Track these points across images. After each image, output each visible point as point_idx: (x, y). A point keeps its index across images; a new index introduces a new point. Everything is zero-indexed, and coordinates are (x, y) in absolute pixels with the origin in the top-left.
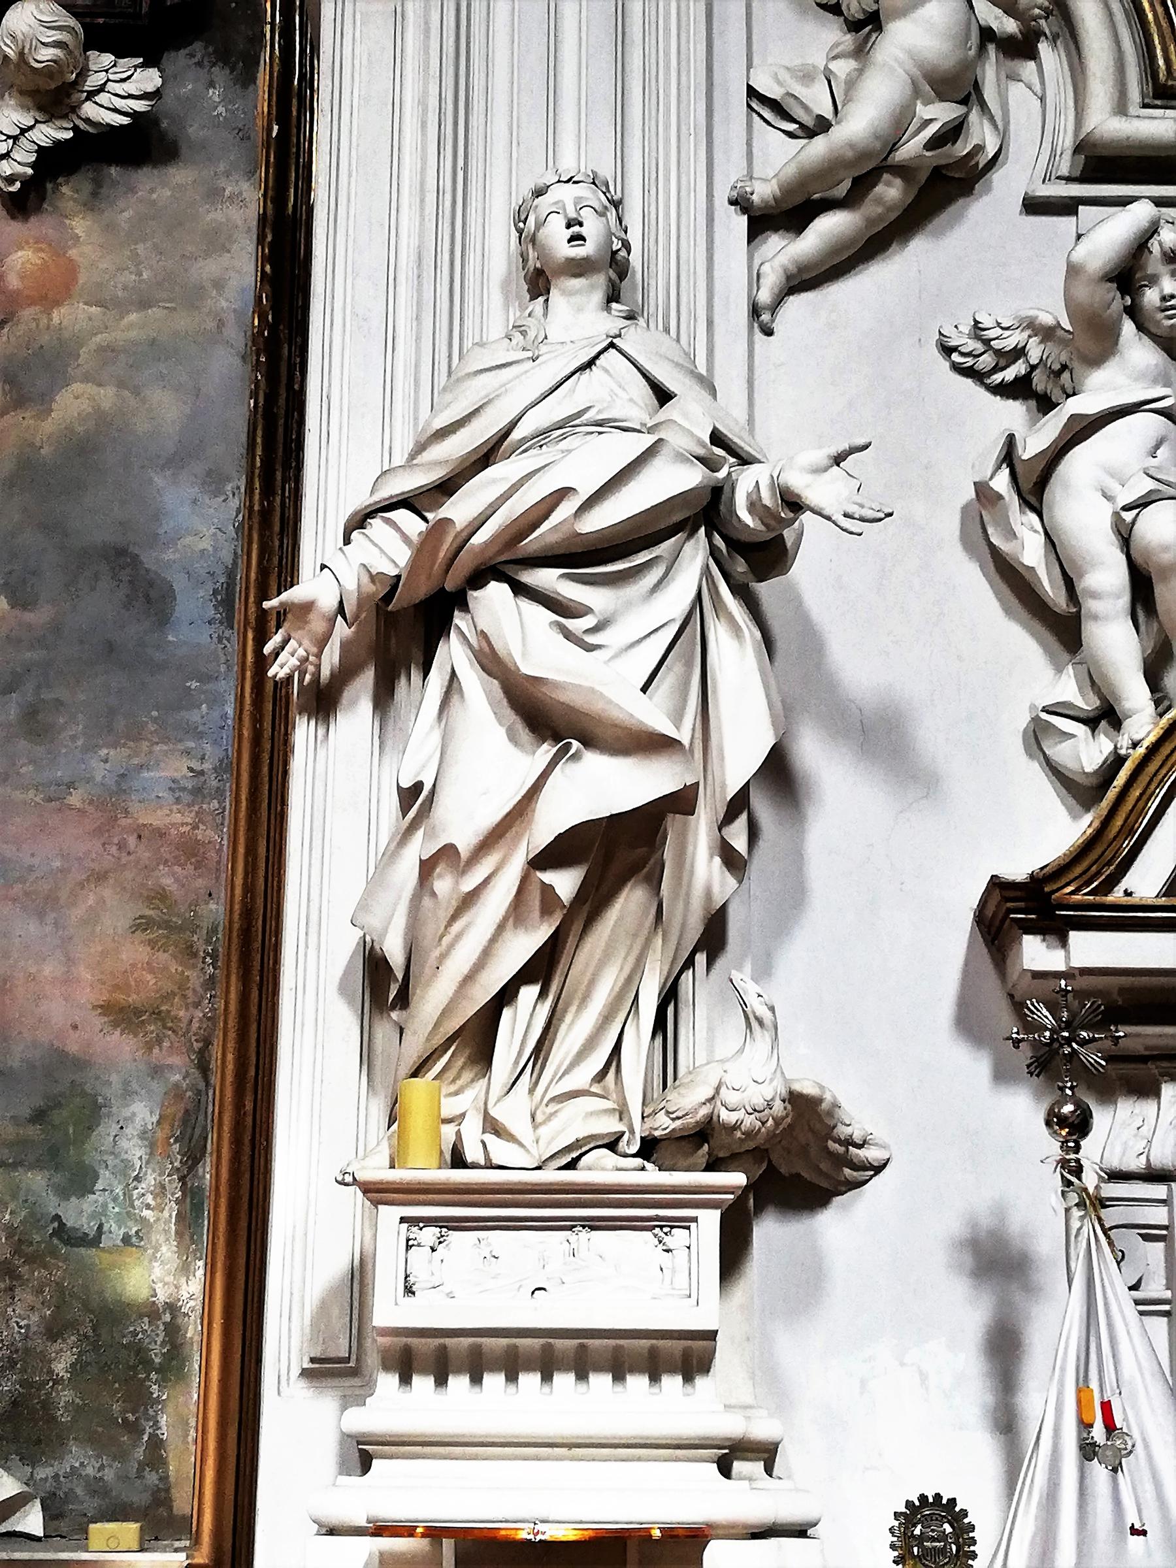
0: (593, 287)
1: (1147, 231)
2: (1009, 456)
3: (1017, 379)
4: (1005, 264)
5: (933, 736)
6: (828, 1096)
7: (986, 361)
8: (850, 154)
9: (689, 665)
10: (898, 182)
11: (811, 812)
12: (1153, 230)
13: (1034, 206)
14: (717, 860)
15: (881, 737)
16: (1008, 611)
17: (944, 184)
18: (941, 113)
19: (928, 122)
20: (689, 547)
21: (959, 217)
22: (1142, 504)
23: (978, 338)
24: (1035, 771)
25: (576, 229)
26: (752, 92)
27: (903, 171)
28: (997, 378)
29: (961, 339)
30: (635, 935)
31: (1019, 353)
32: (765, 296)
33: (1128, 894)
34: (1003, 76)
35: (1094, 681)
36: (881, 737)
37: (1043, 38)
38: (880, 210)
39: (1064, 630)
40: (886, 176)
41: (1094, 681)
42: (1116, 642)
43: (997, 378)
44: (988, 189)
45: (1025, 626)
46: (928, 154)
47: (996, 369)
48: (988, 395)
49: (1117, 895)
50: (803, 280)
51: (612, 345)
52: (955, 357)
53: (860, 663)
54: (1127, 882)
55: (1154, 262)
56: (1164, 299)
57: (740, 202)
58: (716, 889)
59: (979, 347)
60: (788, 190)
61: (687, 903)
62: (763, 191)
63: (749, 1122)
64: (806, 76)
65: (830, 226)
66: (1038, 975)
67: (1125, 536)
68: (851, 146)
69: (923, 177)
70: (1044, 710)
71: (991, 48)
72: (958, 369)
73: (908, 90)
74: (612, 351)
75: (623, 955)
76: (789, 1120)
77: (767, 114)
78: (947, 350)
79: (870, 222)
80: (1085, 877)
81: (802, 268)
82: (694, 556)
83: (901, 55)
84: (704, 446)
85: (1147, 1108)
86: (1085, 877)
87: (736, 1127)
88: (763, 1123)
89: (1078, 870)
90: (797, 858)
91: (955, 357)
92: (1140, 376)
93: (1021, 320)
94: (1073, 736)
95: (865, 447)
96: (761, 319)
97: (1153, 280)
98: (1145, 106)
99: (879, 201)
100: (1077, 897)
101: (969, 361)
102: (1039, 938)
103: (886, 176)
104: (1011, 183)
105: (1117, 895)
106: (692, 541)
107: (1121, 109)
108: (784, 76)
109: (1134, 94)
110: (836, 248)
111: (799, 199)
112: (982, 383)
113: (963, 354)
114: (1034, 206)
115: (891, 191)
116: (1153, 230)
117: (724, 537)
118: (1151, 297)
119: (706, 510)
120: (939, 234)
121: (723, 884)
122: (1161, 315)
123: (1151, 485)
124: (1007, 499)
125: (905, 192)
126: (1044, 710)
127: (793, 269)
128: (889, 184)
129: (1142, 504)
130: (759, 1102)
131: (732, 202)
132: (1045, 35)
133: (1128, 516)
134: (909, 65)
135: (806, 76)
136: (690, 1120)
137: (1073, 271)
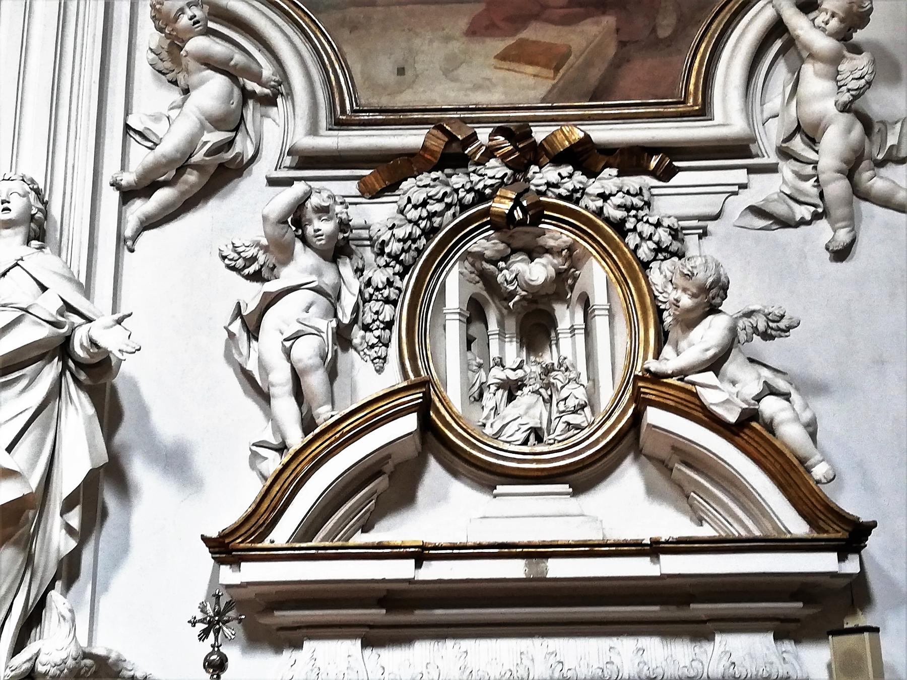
0: (16, 234)
1: (302, 198)
2: (238, 312)
3: (255, 272)
4: (247, 211)
5: (202, 461)
6: (113, 656)
7: (240, 263)
8: (179, 155)
9: (46, 429)
10: (195, 172)
11: (135, 501)
12: (307, 196)
13: (273, 182)
14: (64, 531)
15: (176, 462)
16: (245, 392)
17: (223, 173)
18: (214, 137)
19: (206, 143)
20: (48, 367)
21: (234, 188)
22: (296, 337)
23: (235, 251)
24: (254, 474)
25: (6, 205)
26: (127, 128)
27: (197, 167)
28: (246, 271)
29: (229, 252)
30: (7, 575)
31: (254, 259)
32: (128, 232)
33: (272, 542)
34: (259, 115)
35: (277, 429)
36: (176, 462)
37: (280, 96)
38: (187, 187)
39: (263, 396)
40: (189, 170)
41: (277, 429)
42: (286, 408)
43: (246, 271)
44: (250, 174)
45: (255, 401)
46: (207, 158)
47: (245, 267)
48: (243, 279)
49: (266, 543)
50: (150, 223)
51: (17, 264)
52: (227, 261)
53: (167, 424)
54: (271, 536)
55: (309, 213)
56: (315, 231)
57: (115, 184)
58: (62, 549)
59: (236, 256)
60: (142, 177)
61: (47, 556)
62: (128, 178)
63: (53, 671)
64: (156, 118)
65: (162, 195)
66: (228, 587)
67: (288, 353)
68: (164, 157)
69: (212, 170)
70: (253, 445)
71: (251, 103)
72: (228, 266)
73: (198, 125)
74: (17, 267)
75: (746, 499)
76: (94, 668)
77: (138, 138)
78: (224, 258)
79: (183, 193)
80: (247, 535)
81: (148, 218)
82: (51, 371)
83: (195, 109)
84: (52, 316)
85: (296, 654)
86: (247, 535)
87: (46, 674)
88: (62, 671)
89: (243, 530)
90: (126, 528)
91: (227, 261)
92: (304, 271)
93: (254, 242)
94: (266, 458)
95: (130, 315)
96: (125, 244)
97: (310, 222)
98: (330, 130)
99: (186, 182)
100: (242, 545)
101: (233, 263)
102: (229, 567)
103: (189, 170)
104: (264, 168)
105: (266, 543)
106: (50, 365)
107: (313, 130)
108: (145, 119)
109: (323, 123)
110: (165, 207)
111: (148, 182)
112: (240, 273)
113: (230, 260)
114: (273, 182)
115: (191, 177)
116: (307, 196)
117: (74, 361)
118: (310, 230)
119: (61, 348)
120: (224, 197)
121: (66, 544)
122: (315, 240)
123: (300, 327)
124: (237, 335)
125: (199, 178)
126: (253, 445)
127: (142, 217)
128: (190, 174)
129: (296, 337)
130: (58, 661)
131: (112, 185)
132: (282, 94)
133: (288, 344)
134: (198, 113)
135: (156, 118)
136: (17, 671)
137: (265, 219)
